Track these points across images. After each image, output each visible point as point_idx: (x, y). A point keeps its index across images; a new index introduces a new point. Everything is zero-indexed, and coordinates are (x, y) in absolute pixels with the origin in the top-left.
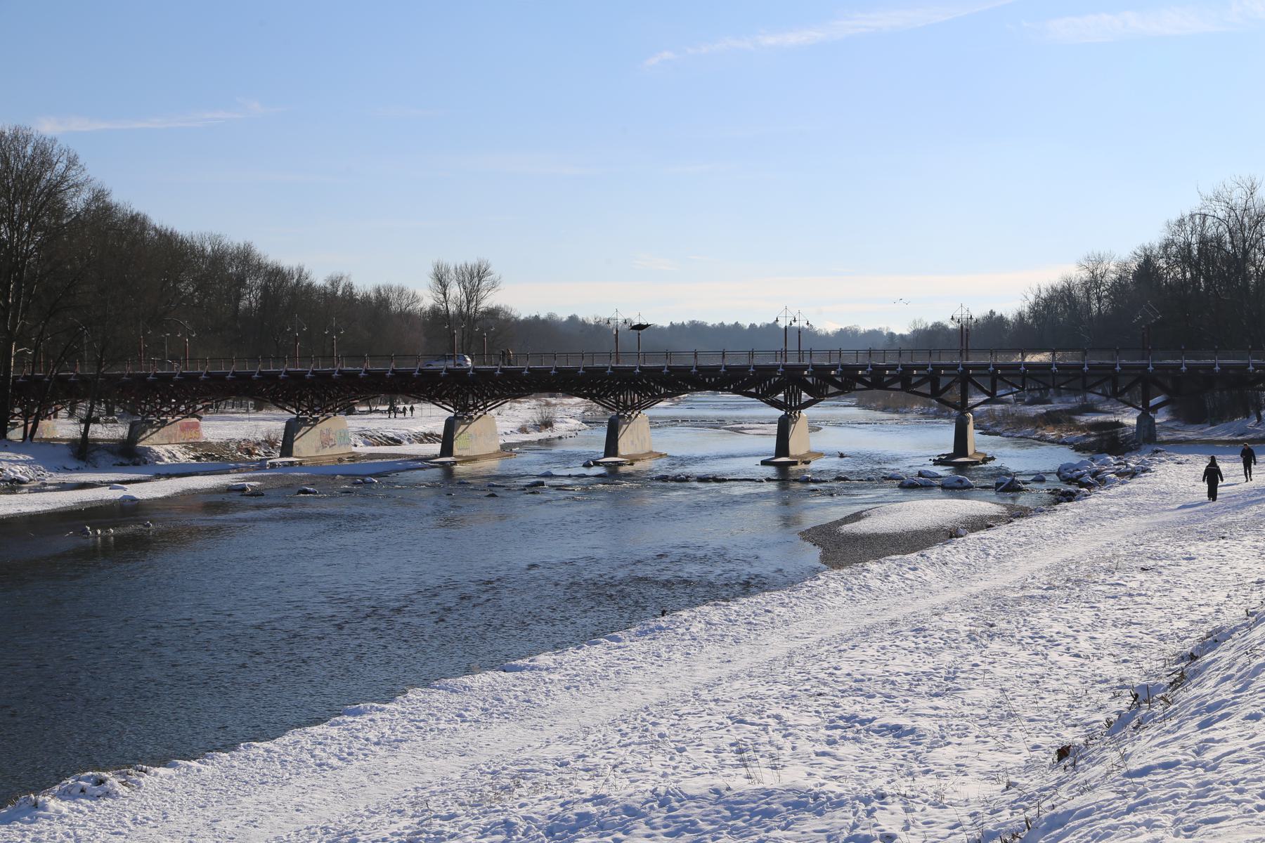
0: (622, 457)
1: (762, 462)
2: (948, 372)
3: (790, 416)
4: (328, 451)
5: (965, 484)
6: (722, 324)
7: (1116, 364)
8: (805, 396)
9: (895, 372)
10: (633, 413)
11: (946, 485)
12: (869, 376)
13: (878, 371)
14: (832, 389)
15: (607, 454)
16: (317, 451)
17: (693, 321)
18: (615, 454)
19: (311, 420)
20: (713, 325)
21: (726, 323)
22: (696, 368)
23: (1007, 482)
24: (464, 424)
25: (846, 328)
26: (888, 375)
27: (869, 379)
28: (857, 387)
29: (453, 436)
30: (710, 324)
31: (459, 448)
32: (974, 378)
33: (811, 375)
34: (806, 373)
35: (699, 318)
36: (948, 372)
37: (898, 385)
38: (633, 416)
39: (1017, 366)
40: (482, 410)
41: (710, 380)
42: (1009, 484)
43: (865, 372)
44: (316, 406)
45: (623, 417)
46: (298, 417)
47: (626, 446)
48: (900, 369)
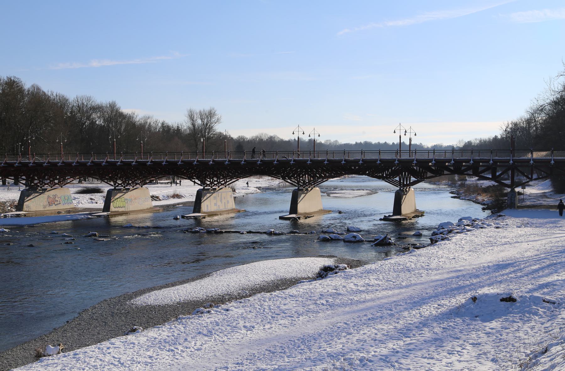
0: (204, 213)
1: (280, 217)
2: (483, 164)
3: (403, 191)
4: (54, 207)
5: (357, 239)
6: (386, 142)
7: (551, 159)
8: (413, 179)
9: (468, 164)
10: (407, 188)
11: (346, 240)
12: (452, 166)
13: (458, 163)
14: (429, 174)
15: (291, 213)
16: (45, 207)
17: (366, 141)
18: (199, 212)
19: (212, 190)
20: (375, 143)
21: (381, 142)
22: (416, 161)
23: (381, 239)
24: (210, 193)
25: (437, 145)
26: (464, 166)
27: (452, 168)
28: (445, 173)
29: (297, 201)
30: (373, 143)
31: (113, 208)
32: (519, 168)
33: (416, 165)
34: (430, 164)
35: (369, 140)
36: (483, 164)
37: (470, 172)
38: (407, 190)
39: (529, 160)
40: (313, 185)
41: (355, 168)
42: (383, 240)
43: (450, 164)
44: (215, 181)
45: (302, 190)
46: (298, 188)
47: (302, 207)
48: (472, 162)
